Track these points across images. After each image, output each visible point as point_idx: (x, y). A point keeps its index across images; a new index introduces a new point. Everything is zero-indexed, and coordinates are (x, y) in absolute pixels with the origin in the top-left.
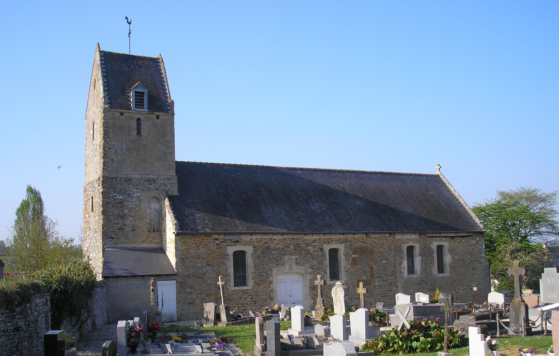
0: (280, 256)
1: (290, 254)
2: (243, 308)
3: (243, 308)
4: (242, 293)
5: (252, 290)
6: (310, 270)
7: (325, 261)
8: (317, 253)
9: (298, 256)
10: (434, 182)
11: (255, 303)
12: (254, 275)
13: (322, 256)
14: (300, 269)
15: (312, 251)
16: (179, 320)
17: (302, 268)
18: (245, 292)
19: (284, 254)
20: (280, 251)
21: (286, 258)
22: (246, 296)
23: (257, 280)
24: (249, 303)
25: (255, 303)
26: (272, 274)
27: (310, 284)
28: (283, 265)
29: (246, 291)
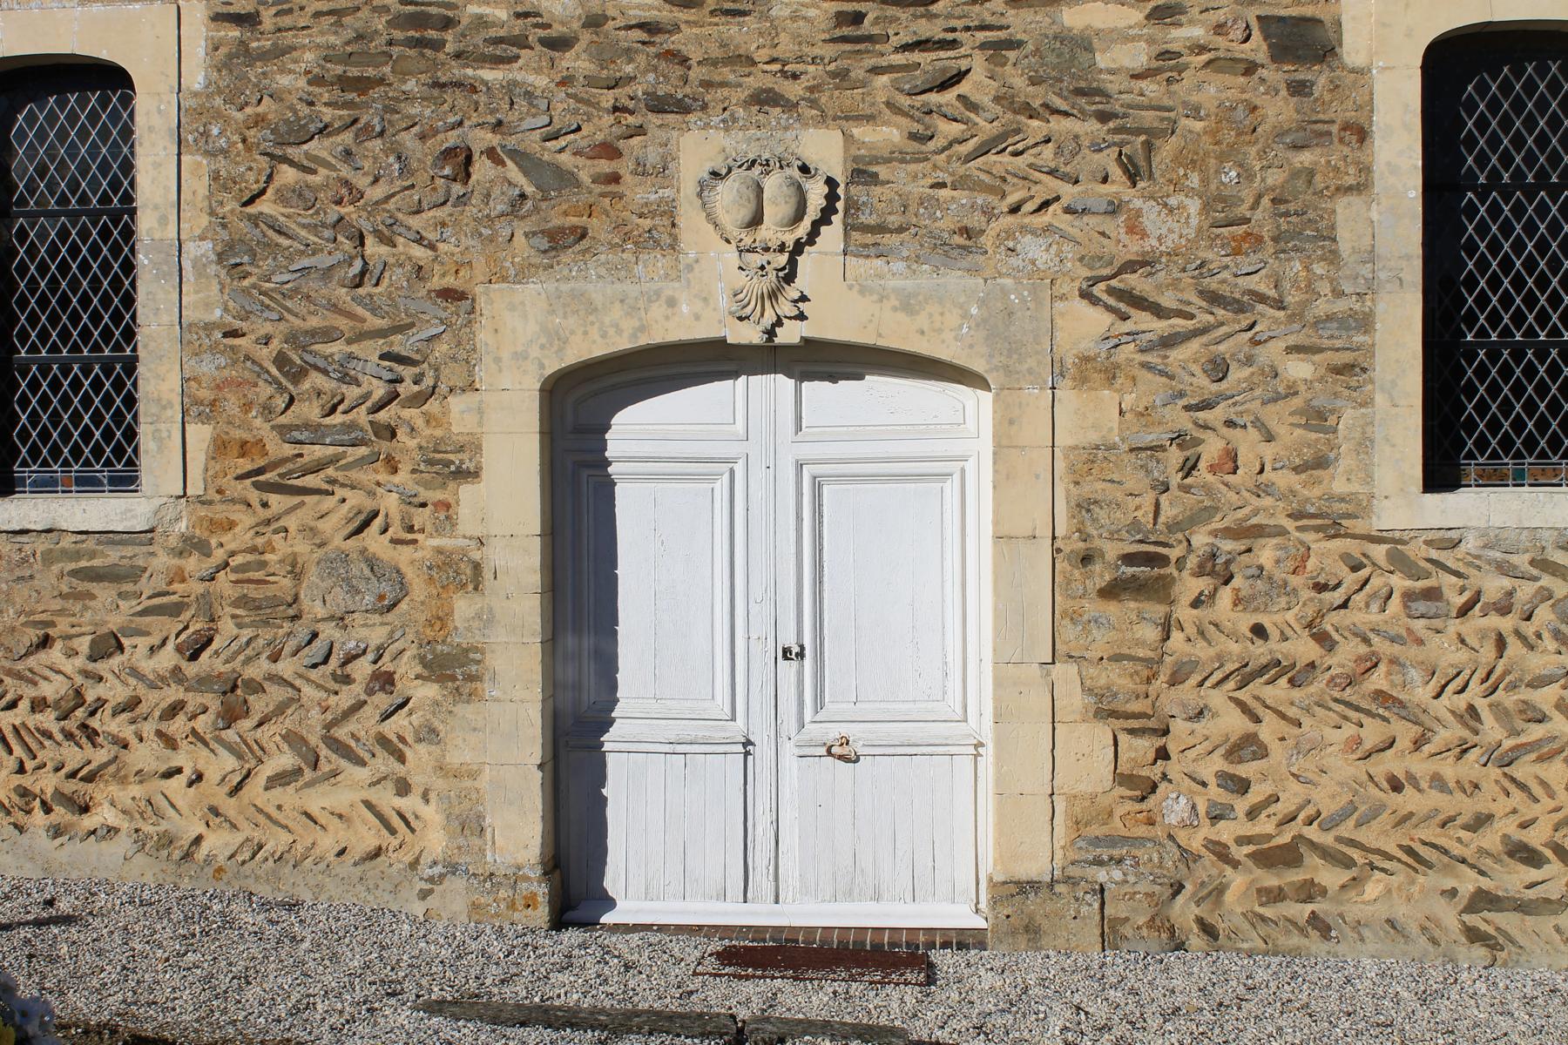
0: (602, 127)
1: (764, 99)
2: (73, 756)
3: (73, 756)
4: (49, 579)
5: (193, 545)
6: (1086, 325)
7: (1346, 211)
8: (1213, 91)
9: (888, 134)
10: (541, 390)
11: (230, 717)
12: (208, 367)
13: (1309, 135)
14: (908, 305)
15: (1137, 56)
16: (870, 163)
17: (955, 280)
18: (97, 566)
19: (659, 105)
20: (604, 54)
21: (697, 148)
22: (108, 608)
23: (261, 427)
24: (156, 700)
25: (230, 717)
26: (467, 358)
27: (1085, 506)
28: (647, 242)
29: (112, 556)
